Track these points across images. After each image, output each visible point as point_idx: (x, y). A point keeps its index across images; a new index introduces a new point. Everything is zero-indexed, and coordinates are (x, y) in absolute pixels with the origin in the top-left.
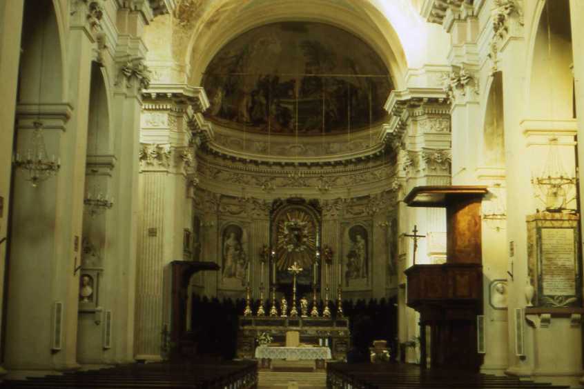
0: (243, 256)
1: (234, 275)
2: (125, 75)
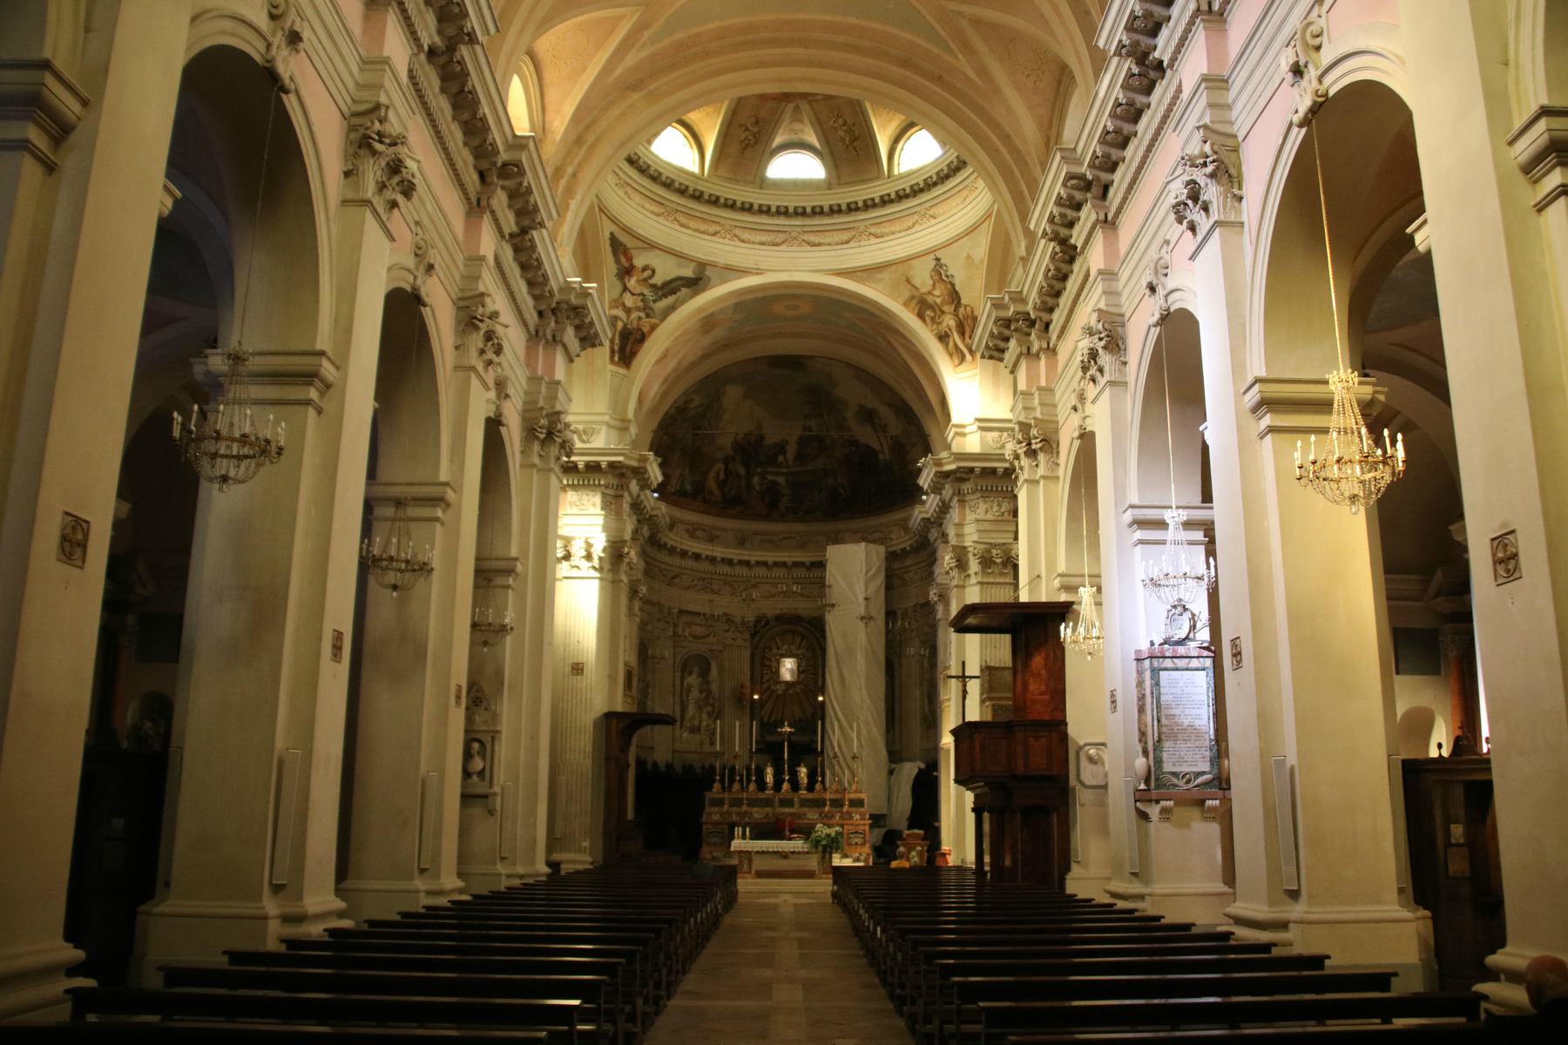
0: (711, 701)
1: (699, 729)
2: (537, 438)
